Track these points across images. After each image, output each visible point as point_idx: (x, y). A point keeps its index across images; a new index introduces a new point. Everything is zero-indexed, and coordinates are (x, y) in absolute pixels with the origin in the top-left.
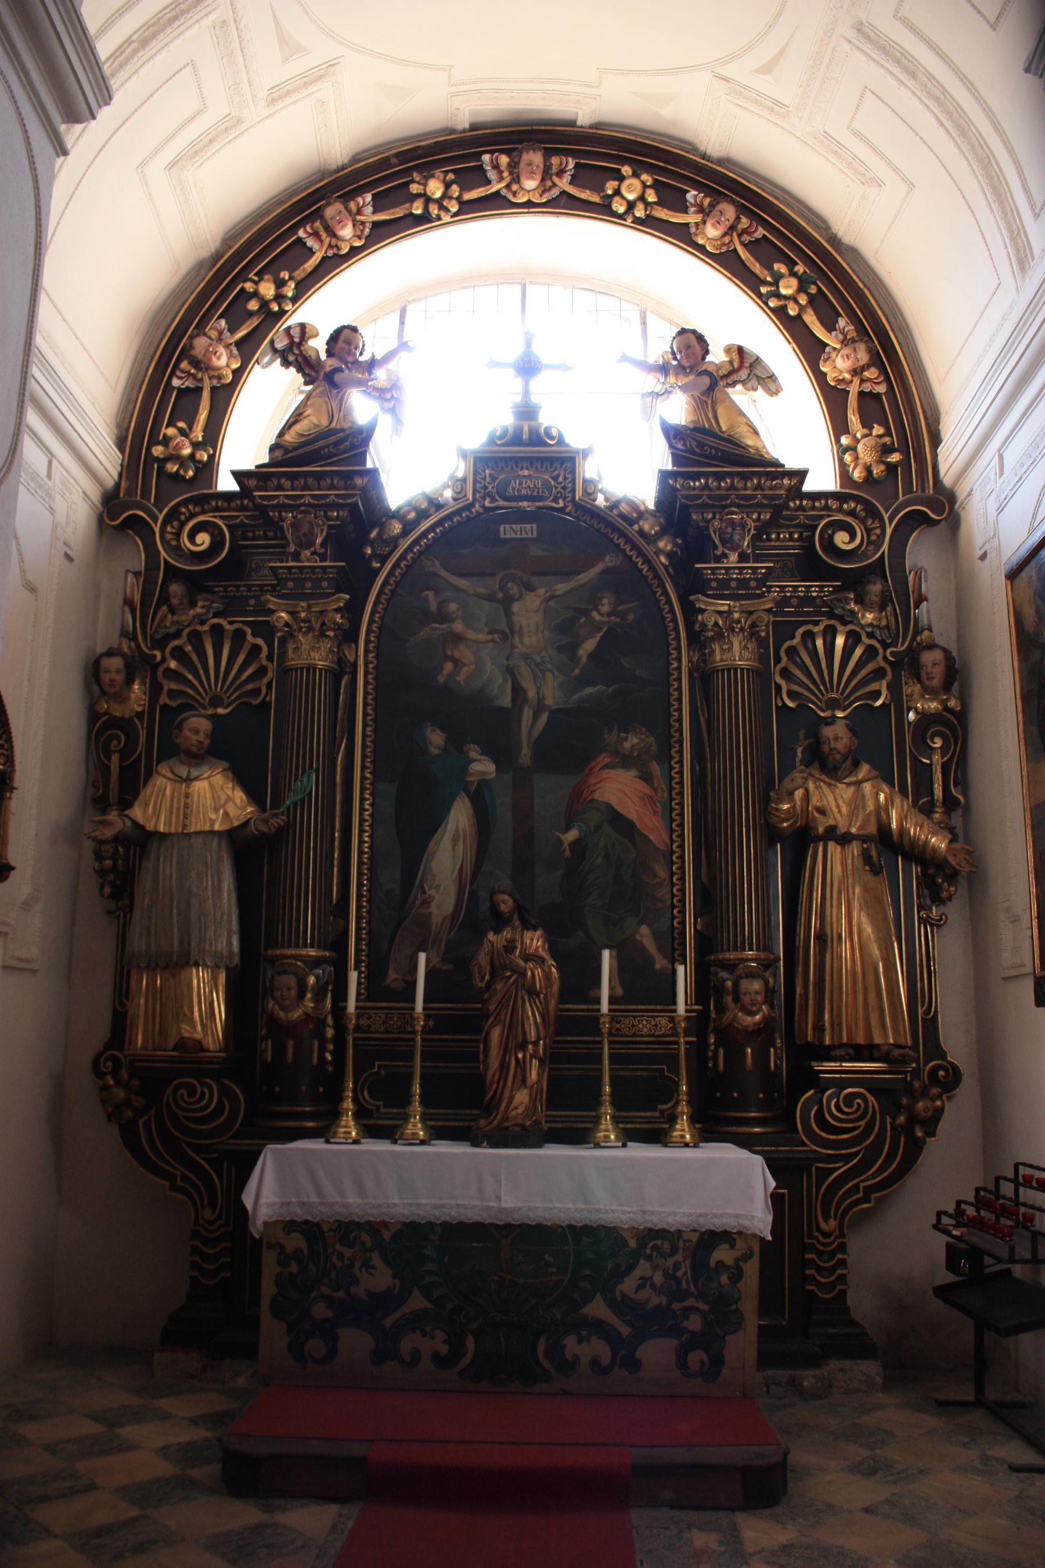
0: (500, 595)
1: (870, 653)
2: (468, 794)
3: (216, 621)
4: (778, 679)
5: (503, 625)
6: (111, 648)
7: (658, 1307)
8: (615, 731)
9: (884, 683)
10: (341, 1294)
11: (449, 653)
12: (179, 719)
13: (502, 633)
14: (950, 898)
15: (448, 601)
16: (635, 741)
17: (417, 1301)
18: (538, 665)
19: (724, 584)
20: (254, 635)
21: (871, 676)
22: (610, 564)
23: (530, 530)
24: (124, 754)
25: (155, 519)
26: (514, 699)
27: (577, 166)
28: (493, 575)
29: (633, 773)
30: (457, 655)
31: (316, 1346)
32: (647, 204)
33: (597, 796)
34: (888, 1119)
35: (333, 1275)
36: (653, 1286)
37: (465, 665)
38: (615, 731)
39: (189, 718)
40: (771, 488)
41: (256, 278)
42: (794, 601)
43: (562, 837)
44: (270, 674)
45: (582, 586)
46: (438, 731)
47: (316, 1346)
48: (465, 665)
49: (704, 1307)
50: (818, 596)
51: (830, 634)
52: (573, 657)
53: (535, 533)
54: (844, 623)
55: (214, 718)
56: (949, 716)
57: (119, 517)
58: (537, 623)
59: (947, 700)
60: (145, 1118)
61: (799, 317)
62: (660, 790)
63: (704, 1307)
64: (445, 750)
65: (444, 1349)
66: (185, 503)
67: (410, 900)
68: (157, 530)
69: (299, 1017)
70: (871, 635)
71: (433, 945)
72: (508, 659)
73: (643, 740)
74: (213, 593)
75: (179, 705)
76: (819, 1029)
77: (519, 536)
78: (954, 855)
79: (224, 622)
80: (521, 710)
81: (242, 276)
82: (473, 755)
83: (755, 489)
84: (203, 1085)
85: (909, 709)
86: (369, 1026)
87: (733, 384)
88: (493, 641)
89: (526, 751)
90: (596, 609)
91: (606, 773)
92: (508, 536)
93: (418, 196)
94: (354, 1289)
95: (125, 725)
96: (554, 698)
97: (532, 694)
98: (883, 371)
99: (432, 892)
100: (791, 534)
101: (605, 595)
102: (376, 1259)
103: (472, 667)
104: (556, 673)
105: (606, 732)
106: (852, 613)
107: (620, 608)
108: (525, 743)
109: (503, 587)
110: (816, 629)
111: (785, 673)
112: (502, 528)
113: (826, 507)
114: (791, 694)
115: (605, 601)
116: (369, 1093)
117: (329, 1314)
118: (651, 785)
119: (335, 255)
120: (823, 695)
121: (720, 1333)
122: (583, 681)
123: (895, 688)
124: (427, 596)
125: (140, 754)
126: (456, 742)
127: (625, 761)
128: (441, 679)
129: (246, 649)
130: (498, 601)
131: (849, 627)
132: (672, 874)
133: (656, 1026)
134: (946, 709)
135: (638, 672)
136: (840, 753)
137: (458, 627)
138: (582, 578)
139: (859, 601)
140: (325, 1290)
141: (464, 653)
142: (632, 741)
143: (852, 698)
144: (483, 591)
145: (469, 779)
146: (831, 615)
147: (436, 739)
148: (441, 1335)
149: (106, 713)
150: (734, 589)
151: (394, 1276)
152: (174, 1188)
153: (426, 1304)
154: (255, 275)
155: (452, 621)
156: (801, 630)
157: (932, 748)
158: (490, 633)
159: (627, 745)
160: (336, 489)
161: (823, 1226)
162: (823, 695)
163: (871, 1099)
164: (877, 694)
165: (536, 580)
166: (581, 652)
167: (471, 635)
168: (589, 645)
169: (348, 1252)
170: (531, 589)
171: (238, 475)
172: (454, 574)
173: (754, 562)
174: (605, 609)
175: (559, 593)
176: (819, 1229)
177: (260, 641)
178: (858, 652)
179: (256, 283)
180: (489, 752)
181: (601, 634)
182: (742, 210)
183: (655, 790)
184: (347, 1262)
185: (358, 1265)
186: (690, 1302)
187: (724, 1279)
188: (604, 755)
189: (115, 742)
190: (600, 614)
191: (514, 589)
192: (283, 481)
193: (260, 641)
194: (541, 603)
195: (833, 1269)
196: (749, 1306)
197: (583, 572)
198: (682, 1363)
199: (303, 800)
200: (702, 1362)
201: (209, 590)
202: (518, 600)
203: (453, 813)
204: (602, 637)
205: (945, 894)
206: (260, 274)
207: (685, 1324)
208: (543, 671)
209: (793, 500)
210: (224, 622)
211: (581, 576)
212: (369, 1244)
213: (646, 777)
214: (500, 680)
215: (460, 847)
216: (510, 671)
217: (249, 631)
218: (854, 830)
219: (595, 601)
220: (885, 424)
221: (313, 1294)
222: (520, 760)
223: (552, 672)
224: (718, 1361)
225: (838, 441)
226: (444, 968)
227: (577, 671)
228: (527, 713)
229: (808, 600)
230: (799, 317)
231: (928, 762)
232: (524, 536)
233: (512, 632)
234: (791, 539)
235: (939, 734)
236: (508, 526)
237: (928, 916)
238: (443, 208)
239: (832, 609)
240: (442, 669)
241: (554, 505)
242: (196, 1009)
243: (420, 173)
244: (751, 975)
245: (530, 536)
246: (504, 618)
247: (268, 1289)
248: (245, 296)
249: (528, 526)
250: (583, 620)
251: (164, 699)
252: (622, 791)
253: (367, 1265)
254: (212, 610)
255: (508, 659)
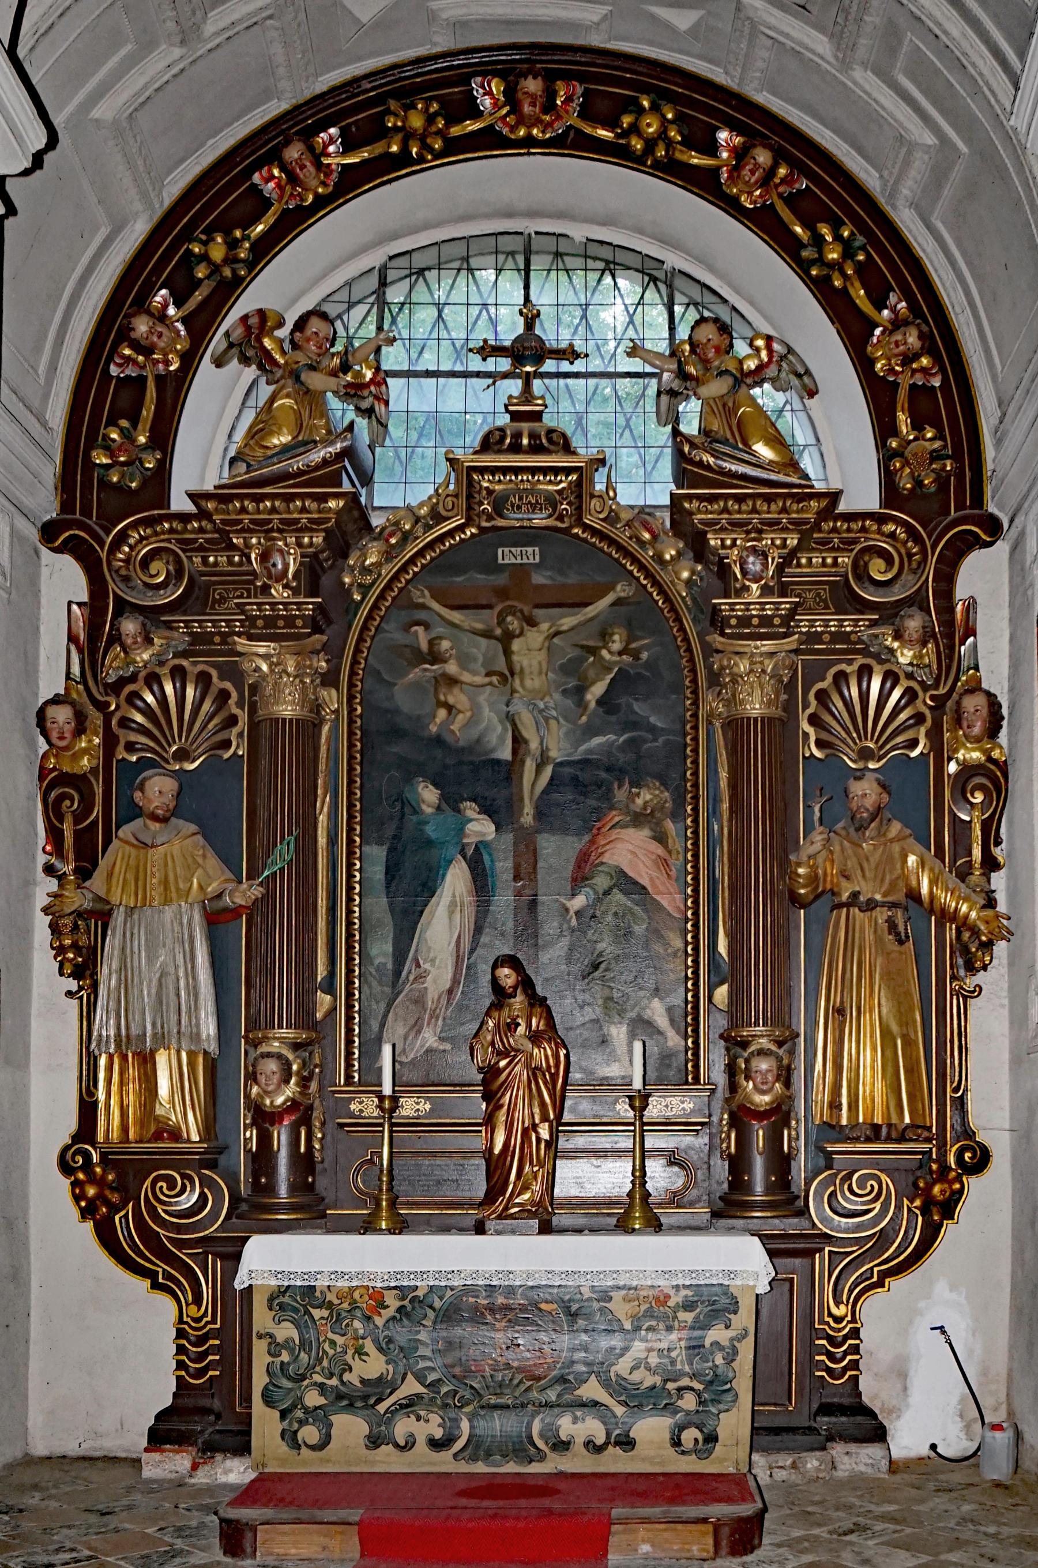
0: (498, 632)
1: (910, 695)
2: (464, 858)
3: (176, 662)
4: (805, 726)
5: (501, 665)
6: (57, 695)
7: (653, 1387)
8: (627, 785)
9: (923, 730)
10: (334, 1382)
11: (442, 698)
12: (140, 778)
13: (501, 675)
14: (985, 968)
15: (440, 638)
16: (648, 797)
17: (411, 1387)
18: (541, 711)
19: (745, 621)
20: (222, 678)
21: (911, 721)
22: (622, 594)
23: (531, 555)
24: (77, 819)
25: (102, 544)
26: (515, 752)
27: (586, 94)
28: (490, 607)
29: (646, 832)
30: (451, 700)
31: (310, 1433)
32: (669, 144)
33: (606, 858)
34: (906, 1202)
35: (325, 1363)
36: (648, 1369)
37: (459, 712)
38: (627, 785)
39: (151, 777)
40: (798, 512)
41: (203, 237)
42: (826, 637)
43: (568, 904)
44: (240, 723)
45: (591, 619)
46: (431, 787)
47: (310, 1433)
48: (459, 712)
49: (699, 1386)
50: (852, 632)
51: (865, 672)
52: (582, 704)
53: (537, 558)
54: (881, 662)
55: (180, 775)
56: (992, 767)
57: (57, 539)
58: (540, 663)
59: (992, 749)
60: (122, 1213)
61: (845, 289)
62: (674, 853)
63: (699, 1386)
64: (439, 808)
65: (438, 1433)
66: (134, 526)
67: (404, 974)
68: (104, 556)
69: (284, 1103)
70: (910, 676)
71: (429, 1024)
72: (507, 705)
73: (656, 796)
74: (171, 629)
75: (139, 759)
76: (835, 1105)
77: (519, 561)
78: (987, 922)
79: (185, 663)
80: (523, 762)
81: (186, 235)
82: (470, 814)
83: (780, 513)
84: (184, 1176)
85: (950, 759)
86: (361, 1111)
87: (759, 383)
88: (490, 684)
89: (528, 811)
90: (605, 647)
91: (615, 834)
92: (506, 561)
93: (396, 129)
94: (346, 1377)
95: (79, 782)
96: (560, 750)
97: (534, 745)
98: (937, 358)
99: (427, 966)
100: (824, 559)
101: (616, 630)
102: (369, 1346)
103: (469, 714)
104: (561, 720)
105: (616, 786)
106: (891, 651)
107: (634, 645)
108: (527, 801)
109: (501, 621)
110: (849, 669)
111: (814, 720)
112: (500, 551)
113: (864, 529)
114: (819, 744)
115: (616, 637)
116: (363, 1182)
117: (322, 1401)
118: (666, 846)
119: (298, 207)
120: (855, 743)
121: (714, 1410)
122: (590, 731)
123: (935, 735)
124: (416, 632)
125: (97, 816)
126: (450, 801)
127: (638, 819)
128: (433, 729)
129: (213, 691)
130: (496, 638)
131: (887, 666)
132: (687, 943)
133: (667, 1106)
134: (990, 759)
135: (652, 719)
136: (867, 810)
137: (452, 668)
138: (591, 611)
139: (898, 636)
140: (318, 1378)
141: (456, 697)
142: (645, 797)
143: (888, 747)
144: (479, 626)
145: (465, 841)
146: (865, 652)
147: (429, 795)
148: (435, 1419)
149: (54, 769)
150: (755, 627)
151: (388, 1363)
152: (155, 1286)
153: (420, 1389)
154: (202, 232)
155: (445, 662)
156: (833, 670)
157: (971, 804)
158: (487, 675)
159: (639, 801)
160: (309, 512)
161: (835, 1311)
162: (855, 743)
163: (884, 1177)
164: (913, 743)
165: (539, 613)
166: (589, 697)
167: (466, 677)
168: (598, 690)
169: (340, 1340)
170: (532, 623)
171: (193, 496)
172: (445, 606)
173: (779, 597)
174: (616, 646)
175: (564, 628)
176: (830, 1314)
177: (228, 685)
178: (896, 694)
179: (205, 243)
180: (488, 810)
181: (612, 675)
182: (780, 156)
183: (670, 852)
184: (339, 1350)
185: (350, 1352)
186: (685, 1382)
187: (719, 1360)
188: (614, 812)
189: (67, 803)
190: (610, 652)
191: (513, 623)
192: (246, 503)
193: (228, 685)
194: (546, 638)
195: (845, 1369)
196: (743, 1386)
197: (590, 604)
198: (676, 1443)
199: (282, 869)
200: (696, 1440)
201: (169, 626)
202: (518, 636)
203: (449, 878)
204: (612, 679)
205: (978, 964)
206: (210, 231)
207: (680, 1403)
208: (547, 719)
209: (825, 520)
210: (185, 663)
211: (590, 608)
212: (361, 1332)
213: (660, 838)
214: (499, 729)
215: (457, 917)
216: (511, 719)
217: (214, 673)
218: (878, 897)
219: (604, 636)
220: (938, 426)
221: (306, 1383)
222: (522, 820)
223: (556, 719)
224: (712, 1439)
225: (884, 444)
226: (441, 1047)
227: (584, 718)
228: (530, 766)
229: (840, 637)
230: (845, 289)
231: (968, 819)
232: (525, 561)
233: (512, 674)
234: (824, 564)
235: (981, 787)
236: (506, 550)
237: (961, 988)
238: (425, 147)
239: (868, 646)
240: (434, 717)
241: (559, 525)
242: (143, 942)
243: (398, 100)
244: (761, 1052)
245: (531, 561)
246: (502, 658)
247: (259, 1380)
248: (189, 261)
249: (530, 550)
250: (592, 659)
251: (121, 753)
252: (633, 853)
253: (360, 1352)
254: (171, 650)
255: (507, 705)
